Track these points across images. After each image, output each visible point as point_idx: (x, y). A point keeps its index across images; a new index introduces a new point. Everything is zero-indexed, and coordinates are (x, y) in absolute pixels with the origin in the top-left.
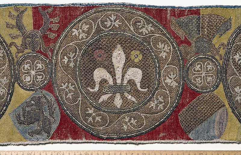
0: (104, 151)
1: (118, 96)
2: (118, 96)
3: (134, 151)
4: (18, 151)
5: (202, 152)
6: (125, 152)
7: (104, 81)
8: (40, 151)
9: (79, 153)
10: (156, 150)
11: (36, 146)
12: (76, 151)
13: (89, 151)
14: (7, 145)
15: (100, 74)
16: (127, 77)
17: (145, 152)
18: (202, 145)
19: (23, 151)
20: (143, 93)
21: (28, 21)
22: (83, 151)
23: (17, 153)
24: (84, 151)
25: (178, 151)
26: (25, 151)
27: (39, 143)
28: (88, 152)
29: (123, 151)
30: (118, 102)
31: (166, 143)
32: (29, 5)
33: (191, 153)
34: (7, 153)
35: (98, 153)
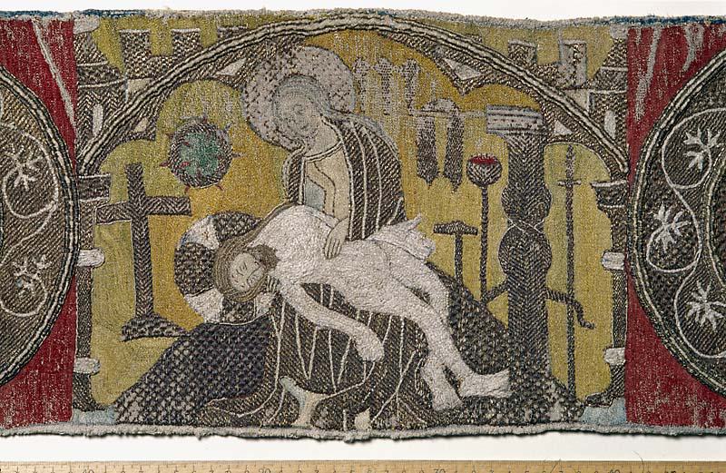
0: (319, 462)
3: (409, 461)
4: (57, 463)
10: (477, 462)
13: (272, 463)
19: (70, 463)
22: (254, 463)
26: (75, 463)
31: (77, 435)
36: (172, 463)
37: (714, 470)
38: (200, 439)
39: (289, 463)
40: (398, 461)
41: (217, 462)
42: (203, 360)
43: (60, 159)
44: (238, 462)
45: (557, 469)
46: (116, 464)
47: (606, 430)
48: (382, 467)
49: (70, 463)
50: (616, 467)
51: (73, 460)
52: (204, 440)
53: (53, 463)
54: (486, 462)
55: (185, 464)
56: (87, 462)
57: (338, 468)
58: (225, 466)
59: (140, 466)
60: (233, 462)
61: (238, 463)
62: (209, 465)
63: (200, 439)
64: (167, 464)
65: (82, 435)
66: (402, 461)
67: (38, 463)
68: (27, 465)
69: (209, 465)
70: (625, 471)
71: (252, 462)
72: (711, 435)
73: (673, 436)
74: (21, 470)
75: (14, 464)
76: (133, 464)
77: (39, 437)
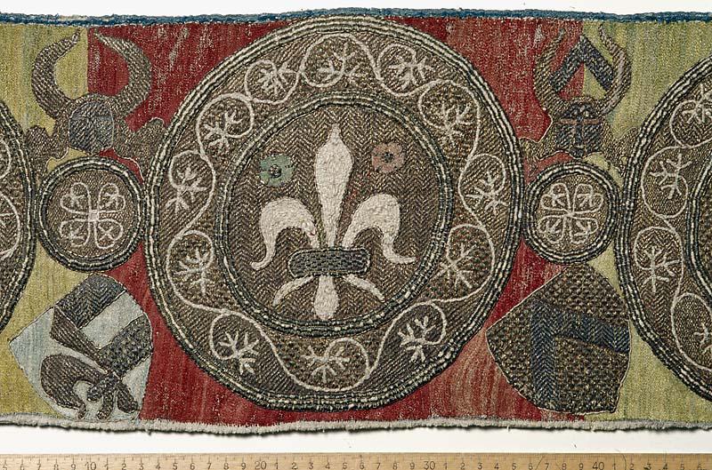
0: (313, 455)
1: (326, 283)
2: (326, 283)
3: (399, 454)
4: (60, 456)
5: (601, 459)
6: (374, 460)
7: (288, 239)
8: (123, 457)
9: (239, 462)
10: (466, 454)
11: (310, 437)
12: (231, 455)
13: (268, 455)
14: (564, 428)
15: (280, 215)
16: (359, 221)
17: (432, 458)
18: (321, 436)
19: (72, 455)
20: (270, 294)
21: (73, 77)
23: (54, 462)
24: (252, 454)
26: (78, 455)
27: (134, 427)
28: (264, 459)
29: (370, 455)
30: (325, 303)
31: (196, 432)
32: (75, 22)
33: (519, 462)
34: (26, 462)
35: (160, 461)
38: (150, 434)
40: (389, 454)
41: (215, 455)
43: (151, 175)
49: (361, 456)
51: (75, 453)
53: (55, 456)
56: (90, 455)
58: (223, 458)
59: (346, 458)
62: (207, 457)
63: (150, 434)
65: (36, 426)
66: (394, 454)
67: (43, 456)
71: (249, 454)
73: (654, 429)
75: (19, 456)
76: (134, 456)
77: (173, 435)
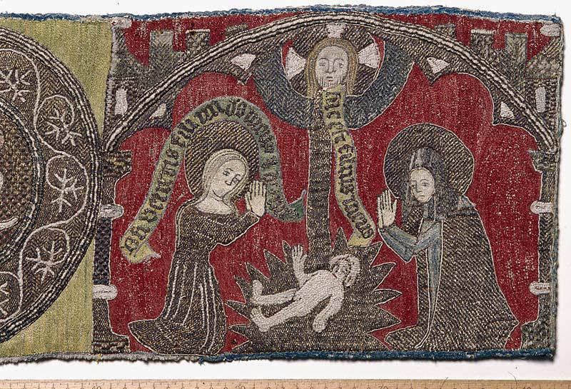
0: (285, 381)
4: (71, 381)
13: (247, 381)
19: (82, 381)
25: (469, 381)
26: (86, 381)
36: (165, 381)
37: (514, 386)
39: (261, 381)
42: (105, 228)
44: (219, 380)
45: (537, 386)
46: (119, 382)
47: (67, 357)
48: (336, 385)
50: (528, 385)
51: (84, 379)
52: (100, 363)
53: (67, 381)
54: (421, 381)
55: (175, 382)
57: (300, 385)
60: (215, 380)
61: (219, 382)
64: (161, 382)
68: (46, 382)
69: (195, 383)
70: (544, 386)
72: (158, 360)
74: (42, 386)
75: (36, 381)
